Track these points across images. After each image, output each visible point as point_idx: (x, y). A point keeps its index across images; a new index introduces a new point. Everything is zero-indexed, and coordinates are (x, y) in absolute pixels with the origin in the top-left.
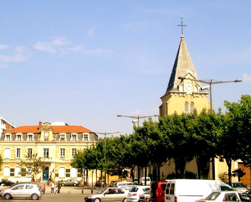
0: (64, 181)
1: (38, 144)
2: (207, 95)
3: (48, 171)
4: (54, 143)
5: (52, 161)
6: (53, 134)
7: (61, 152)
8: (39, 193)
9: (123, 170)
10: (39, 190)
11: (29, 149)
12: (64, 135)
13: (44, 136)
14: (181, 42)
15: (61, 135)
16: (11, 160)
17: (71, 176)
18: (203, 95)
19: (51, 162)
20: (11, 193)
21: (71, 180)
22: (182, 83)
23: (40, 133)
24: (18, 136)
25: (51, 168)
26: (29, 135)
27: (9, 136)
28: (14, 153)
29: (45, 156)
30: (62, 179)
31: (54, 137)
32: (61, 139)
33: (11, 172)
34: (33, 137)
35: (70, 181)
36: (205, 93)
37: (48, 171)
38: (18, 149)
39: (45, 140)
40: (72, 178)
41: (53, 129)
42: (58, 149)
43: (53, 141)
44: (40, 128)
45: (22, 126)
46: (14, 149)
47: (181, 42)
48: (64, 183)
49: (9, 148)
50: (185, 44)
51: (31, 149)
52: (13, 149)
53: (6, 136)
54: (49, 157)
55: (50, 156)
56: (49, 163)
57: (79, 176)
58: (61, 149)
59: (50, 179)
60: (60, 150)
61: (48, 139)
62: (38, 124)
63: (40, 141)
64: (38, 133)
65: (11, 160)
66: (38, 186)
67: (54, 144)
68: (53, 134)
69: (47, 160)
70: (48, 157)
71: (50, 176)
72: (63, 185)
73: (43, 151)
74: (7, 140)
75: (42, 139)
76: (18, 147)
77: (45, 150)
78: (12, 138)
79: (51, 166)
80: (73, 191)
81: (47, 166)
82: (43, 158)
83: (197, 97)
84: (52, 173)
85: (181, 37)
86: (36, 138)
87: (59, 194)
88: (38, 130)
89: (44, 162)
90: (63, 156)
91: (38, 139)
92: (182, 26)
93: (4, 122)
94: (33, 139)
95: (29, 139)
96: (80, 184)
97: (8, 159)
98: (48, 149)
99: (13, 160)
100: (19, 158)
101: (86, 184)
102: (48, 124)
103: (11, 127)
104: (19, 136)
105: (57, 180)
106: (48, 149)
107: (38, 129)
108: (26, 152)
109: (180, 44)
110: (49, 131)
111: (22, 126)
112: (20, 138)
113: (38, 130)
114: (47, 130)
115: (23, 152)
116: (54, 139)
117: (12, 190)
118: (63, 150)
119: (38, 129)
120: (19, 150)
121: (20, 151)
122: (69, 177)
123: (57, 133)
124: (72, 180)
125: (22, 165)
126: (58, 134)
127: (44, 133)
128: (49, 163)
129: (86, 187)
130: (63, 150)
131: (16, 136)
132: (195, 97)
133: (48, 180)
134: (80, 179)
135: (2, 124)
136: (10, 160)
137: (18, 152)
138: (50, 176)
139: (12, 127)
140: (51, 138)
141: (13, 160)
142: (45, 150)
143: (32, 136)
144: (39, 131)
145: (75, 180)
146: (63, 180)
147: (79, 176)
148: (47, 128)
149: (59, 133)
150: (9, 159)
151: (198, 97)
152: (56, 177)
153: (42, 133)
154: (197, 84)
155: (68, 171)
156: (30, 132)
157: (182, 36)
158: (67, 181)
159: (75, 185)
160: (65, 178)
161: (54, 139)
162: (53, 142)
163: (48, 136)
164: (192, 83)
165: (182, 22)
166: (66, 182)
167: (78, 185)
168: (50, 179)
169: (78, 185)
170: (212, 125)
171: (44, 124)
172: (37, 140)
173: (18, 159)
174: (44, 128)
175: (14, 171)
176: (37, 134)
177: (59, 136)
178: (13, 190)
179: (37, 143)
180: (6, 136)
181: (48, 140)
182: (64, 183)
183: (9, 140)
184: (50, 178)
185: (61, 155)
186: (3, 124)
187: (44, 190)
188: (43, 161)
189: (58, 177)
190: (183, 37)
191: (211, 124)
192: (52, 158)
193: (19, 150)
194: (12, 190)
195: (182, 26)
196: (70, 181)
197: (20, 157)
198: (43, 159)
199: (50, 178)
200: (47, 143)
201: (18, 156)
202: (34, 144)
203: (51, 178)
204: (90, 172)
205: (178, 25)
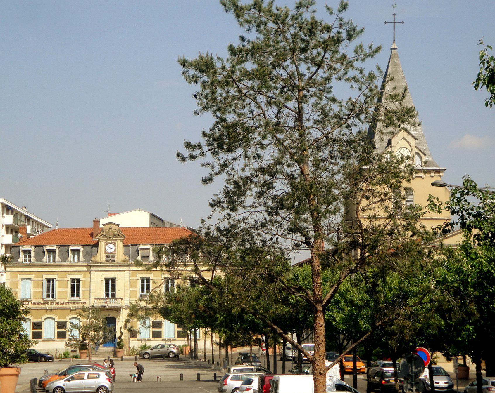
0: (149, 348)
1: (92, 269)
2: (442, 174)
3: (113, 327)
4: (127, 266)
5: (123, 305)
6: (124, 246)
7: (143, 286)
8: (107, 384)
9: (254, 338)
10: (110, 381)
11: (73, 280)
12: (149, 249)
13: (106, 252)
14: (390, 60)
15: (141, 249)
16: (34, 304)
17: (164, 335)
18: (433, 174)
19: (122, 307)
20: (63, 386)
21: (163, 346)
22: (390, 150)
23: (96, 245)
24: (49, 251)
25: (120, 320)
26: (72, 250)
27: (29, 252)
28: (41, 290)
29: (108, 295)
30: (142, 344)
31: (126, 254)
32: (142, 257)
33: (33, 329)
34: (81, 253)
35: (161, 348)
36: (438, 168)
37: (113, 326)
38: (48, 281)
39: (107, 260)
40: (166, 340)
41: (125, 237)
42: (135, 278)
43: (124, 261)
44: (97, 235)
45: (57, 228)
46: (41, 279)
47: (390, 60)
48: (148, 353)
49: (30, 279)
50: (400, 64)
51: (78, 280)
52: (36, 279)
53: (21, 253)
54: (117, 297)
55: (118, 294)
56: (118, 310)
57: (179, 335)
58: (143, 280)
59: (119, 344)
60: (140, 281)
61: (113, 257)
62: (91, 225)
63: (96, 262)
64: (92, 244)
65: (34, 304)
66: (106, 375)
67: (127, 268)
68: (124, 246)
69: (111, 303)
70: (113, 296)
71: (120, 338)
72: (147, 356)
73: (104, 283)
74: (25, 261)
75: (101, 257)
76: (50, 277)
77: (107, 280)
78: (35, 256)
79: (121, 316)
80: (165, 373)
81: (112, 314)
82: (103, 299)
83: (421, 178)
84: (123, 330)
85: (392, 49)
86: (87, 255)
87: (140, 381)
88: (92, 237)
89: (104, 307)
90: (145, 293)
91: (93, 259)
92: (394, 23)
93: (8, 209)
94: (82, 259)
95: (72, 258)
96: (182, 352)
97: (27, 303)
98: (114, 280)
99: (38, 304)
100: (51, 298)
101: (193, 354)
102: (113, 227)
103: (23, 219)
104: (51, 252)
105: (135, 344)
106: (114, 280)
107: (92, 235)
108: (67, 287)
109: (389, 64)
110: (116, 240)
111: (55, 230)
112: (54, 256)
113: (92, 237)
114: (111, 238)
115: (59, 287)
116: (127, 258)
117: (65, 381)
118: (145, 281)
119: (92, 235)
120: (51, 282)
121: (53, 285)
122: (161, 338)
123: (132, 245)
124: (166, 346)
125: (72, 330)
126: (135, 247)
127: (105, 246)
128: (118, 310)
129: (193, 362)
130: (145, 281)
131: (44, 252)
132: (416, 177)
133: (115, 346)
134: (181, 342)
135: (3, 214)
136: (32, 304)
137: (48, 288)
138: (120, 338)
139: (25, 218)
140: (120, 256)
141: (38, 304)
142: (107, 280)
143: (78, 250)
144: (95, 240)
145: (172, 346)
146: (148, 345)
147: (179, 335)
148: (111, 234)
149: (137, 245)
150: (30, 303)
151: (423, 178)
152: (131, 339)
153: (102, 244)
154: (420, 150)
155: (157, 325)
156: (75, 243)
157: (393, 47)
158: (156, 347)
159: (172, 355)
160: (150, 340)
161: (127, 258)
162: (125, 264)
163: (115, 252)
164: (410, 149)
165: (394, 15)
166: (152, 349)
167: (176, 357)
168: (119, 344)
169: (178, 356)
170: (340, 302)
171: (104, 225)
172: (90, 260)
173: (50, 302)
174: (104, 233)
175: (41, 329)
176: (90, 247)
177: (137, 251)
178: (68, 382)
179: (90, 266)
180: (21, 253)
181: (113, 260)
182: (149, 351)
183: (30, 261)
184: (118, 340)
185: (143, 291)
186: (5, 214)
187: (114, 376)
188: (104, 305)
189: (136, 339)
190: (396, 47)
191: (339, 299)
192: (122, 299)
193: (51, 282)
194: (65, 381)
195: (394, 23)
196: (161, 348)
197: (53, 296)
198: (104, 301)
199: (118, 340)
200: (112, 266)
201: (48, 296)
202: (84, 269)
203: (121, 340)
204: (200, 332)
205: (386, 23)
